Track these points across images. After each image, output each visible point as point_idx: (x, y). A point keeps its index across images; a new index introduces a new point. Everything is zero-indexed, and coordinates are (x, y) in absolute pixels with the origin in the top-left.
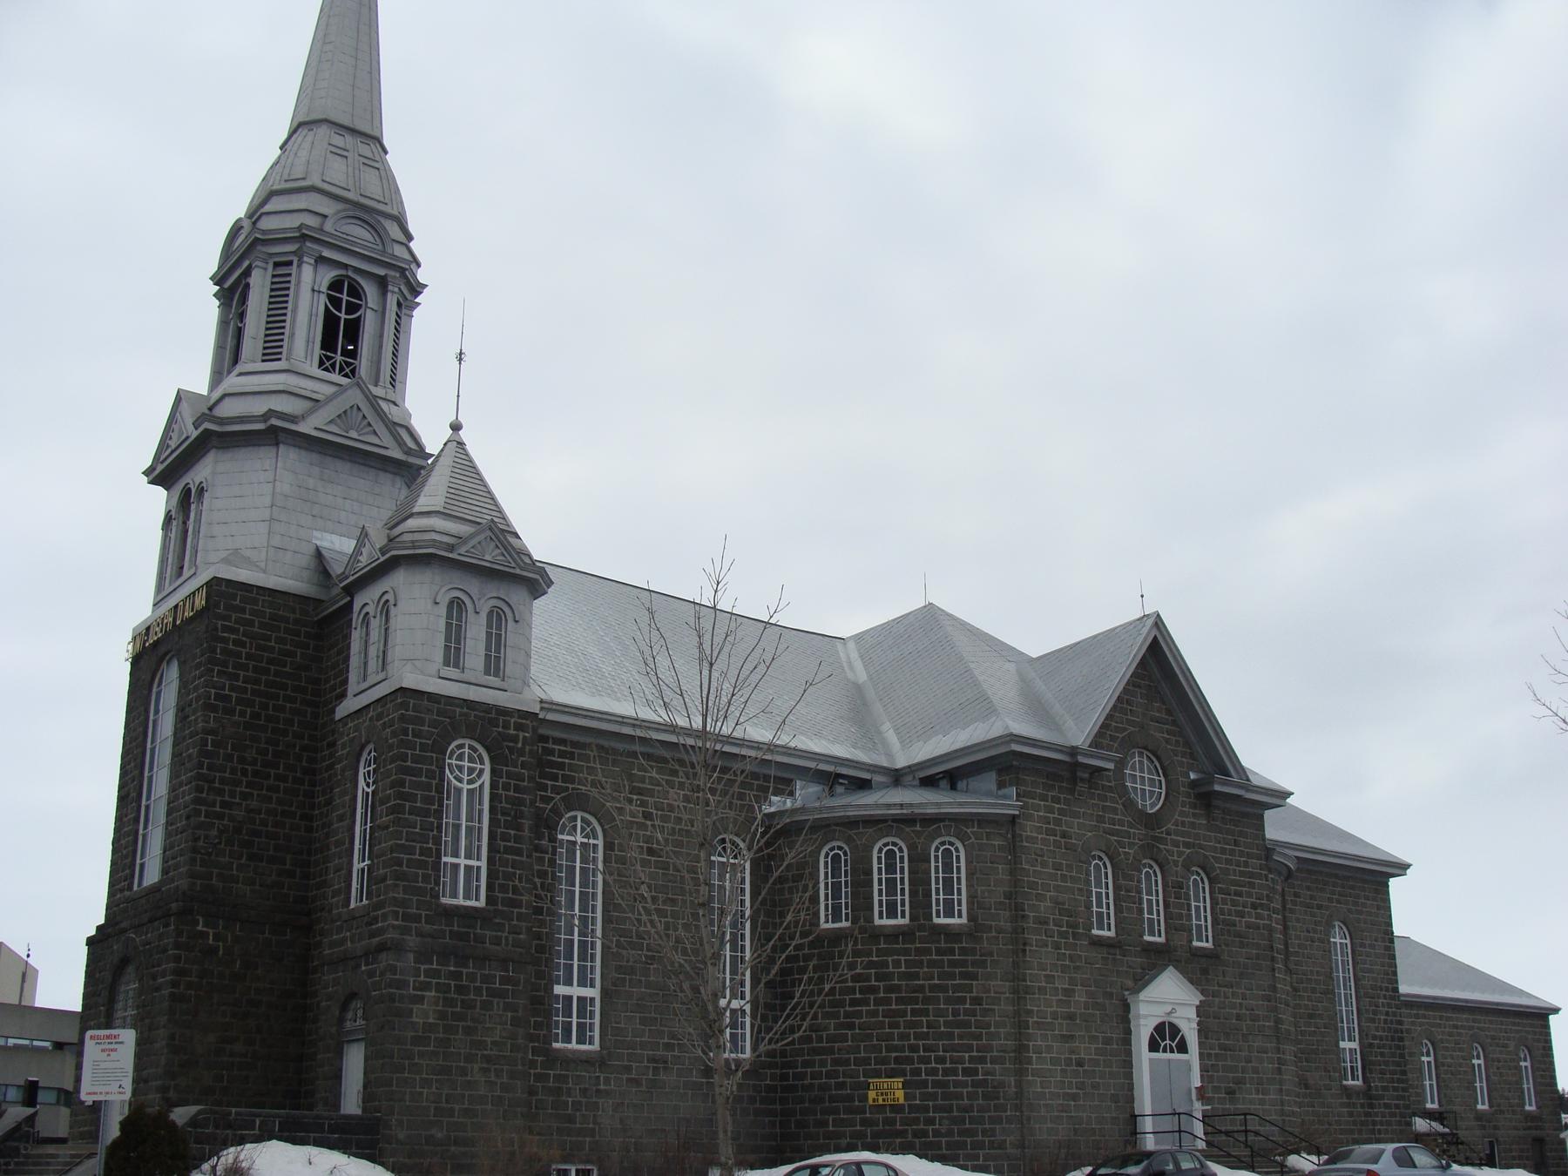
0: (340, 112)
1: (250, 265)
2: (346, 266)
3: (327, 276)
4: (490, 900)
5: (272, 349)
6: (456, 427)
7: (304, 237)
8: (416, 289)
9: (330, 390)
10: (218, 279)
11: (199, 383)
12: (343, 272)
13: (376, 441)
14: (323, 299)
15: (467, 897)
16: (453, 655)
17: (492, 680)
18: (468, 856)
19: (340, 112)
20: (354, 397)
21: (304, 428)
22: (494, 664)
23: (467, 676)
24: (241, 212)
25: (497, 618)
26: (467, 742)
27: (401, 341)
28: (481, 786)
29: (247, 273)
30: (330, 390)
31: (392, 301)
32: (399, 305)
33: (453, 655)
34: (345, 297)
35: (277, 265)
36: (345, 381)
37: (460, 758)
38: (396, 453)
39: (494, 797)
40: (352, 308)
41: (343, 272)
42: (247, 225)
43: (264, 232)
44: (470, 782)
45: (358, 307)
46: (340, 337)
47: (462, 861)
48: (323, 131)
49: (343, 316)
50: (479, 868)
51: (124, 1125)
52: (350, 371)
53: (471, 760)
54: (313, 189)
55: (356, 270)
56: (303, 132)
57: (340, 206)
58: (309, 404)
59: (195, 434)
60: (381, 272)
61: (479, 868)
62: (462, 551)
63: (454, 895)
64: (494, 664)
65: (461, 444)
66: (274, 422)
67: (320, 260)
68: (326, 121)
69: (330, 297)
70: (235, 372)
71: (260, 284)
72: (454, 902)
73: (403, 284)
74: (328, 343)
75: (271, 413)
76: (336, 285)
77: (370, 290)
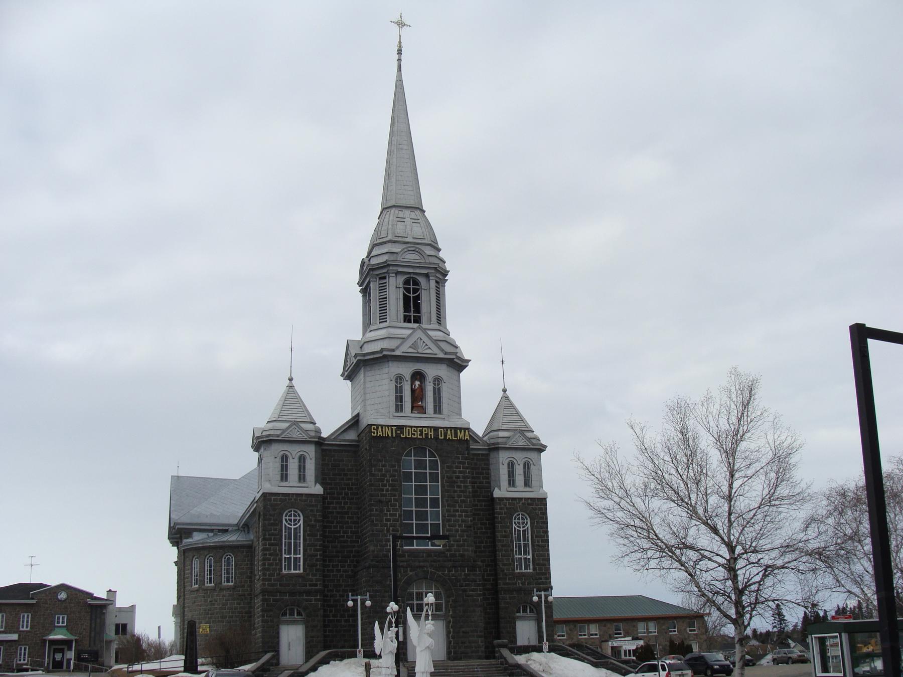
0: (402, 199)
1: (372, 275)
2: (410, 273)
3: (401, 279)
4: (534, 569)
5: (383, 319)
6: (291, 380)
8: (445, 273)
9: (409, 332)
10: (360, 284)
11: (358, 336)
14: (401, 291)
17: (528, 489)
19: (402, 199)
20: (419, 334)
21: (398, 353)
22: (527, 483)
24: (364, 255)
27: (441, 296)
29: (369, 283)
30: (409, 332)
31: (433, 284)
32: (437, 282)
34: (411, 287)
35: (380, 278)
36: (416, 325)
38: (441, 355)
40: (415, 291)
42: (366, 260)
46: (412, 309)
47: (523, 556)
48: (393, 210)
49: (412, 295)
51: (518, 666)
52: (417, 320)
53: (523, 519)
54: (390, 241)
55: (414, 273)
57: (405, 246)
60: (425, 271)
64: (527, 483)
65: (507, 397)
66: (385, 353)
67: (398, 273)
68: (394, 206)
69: (405, 288)
71: (374, 286)
73: (439, 274)
74: (407, 308)
75: (382, 350)
76: (407, 282)
77: (422, 281)
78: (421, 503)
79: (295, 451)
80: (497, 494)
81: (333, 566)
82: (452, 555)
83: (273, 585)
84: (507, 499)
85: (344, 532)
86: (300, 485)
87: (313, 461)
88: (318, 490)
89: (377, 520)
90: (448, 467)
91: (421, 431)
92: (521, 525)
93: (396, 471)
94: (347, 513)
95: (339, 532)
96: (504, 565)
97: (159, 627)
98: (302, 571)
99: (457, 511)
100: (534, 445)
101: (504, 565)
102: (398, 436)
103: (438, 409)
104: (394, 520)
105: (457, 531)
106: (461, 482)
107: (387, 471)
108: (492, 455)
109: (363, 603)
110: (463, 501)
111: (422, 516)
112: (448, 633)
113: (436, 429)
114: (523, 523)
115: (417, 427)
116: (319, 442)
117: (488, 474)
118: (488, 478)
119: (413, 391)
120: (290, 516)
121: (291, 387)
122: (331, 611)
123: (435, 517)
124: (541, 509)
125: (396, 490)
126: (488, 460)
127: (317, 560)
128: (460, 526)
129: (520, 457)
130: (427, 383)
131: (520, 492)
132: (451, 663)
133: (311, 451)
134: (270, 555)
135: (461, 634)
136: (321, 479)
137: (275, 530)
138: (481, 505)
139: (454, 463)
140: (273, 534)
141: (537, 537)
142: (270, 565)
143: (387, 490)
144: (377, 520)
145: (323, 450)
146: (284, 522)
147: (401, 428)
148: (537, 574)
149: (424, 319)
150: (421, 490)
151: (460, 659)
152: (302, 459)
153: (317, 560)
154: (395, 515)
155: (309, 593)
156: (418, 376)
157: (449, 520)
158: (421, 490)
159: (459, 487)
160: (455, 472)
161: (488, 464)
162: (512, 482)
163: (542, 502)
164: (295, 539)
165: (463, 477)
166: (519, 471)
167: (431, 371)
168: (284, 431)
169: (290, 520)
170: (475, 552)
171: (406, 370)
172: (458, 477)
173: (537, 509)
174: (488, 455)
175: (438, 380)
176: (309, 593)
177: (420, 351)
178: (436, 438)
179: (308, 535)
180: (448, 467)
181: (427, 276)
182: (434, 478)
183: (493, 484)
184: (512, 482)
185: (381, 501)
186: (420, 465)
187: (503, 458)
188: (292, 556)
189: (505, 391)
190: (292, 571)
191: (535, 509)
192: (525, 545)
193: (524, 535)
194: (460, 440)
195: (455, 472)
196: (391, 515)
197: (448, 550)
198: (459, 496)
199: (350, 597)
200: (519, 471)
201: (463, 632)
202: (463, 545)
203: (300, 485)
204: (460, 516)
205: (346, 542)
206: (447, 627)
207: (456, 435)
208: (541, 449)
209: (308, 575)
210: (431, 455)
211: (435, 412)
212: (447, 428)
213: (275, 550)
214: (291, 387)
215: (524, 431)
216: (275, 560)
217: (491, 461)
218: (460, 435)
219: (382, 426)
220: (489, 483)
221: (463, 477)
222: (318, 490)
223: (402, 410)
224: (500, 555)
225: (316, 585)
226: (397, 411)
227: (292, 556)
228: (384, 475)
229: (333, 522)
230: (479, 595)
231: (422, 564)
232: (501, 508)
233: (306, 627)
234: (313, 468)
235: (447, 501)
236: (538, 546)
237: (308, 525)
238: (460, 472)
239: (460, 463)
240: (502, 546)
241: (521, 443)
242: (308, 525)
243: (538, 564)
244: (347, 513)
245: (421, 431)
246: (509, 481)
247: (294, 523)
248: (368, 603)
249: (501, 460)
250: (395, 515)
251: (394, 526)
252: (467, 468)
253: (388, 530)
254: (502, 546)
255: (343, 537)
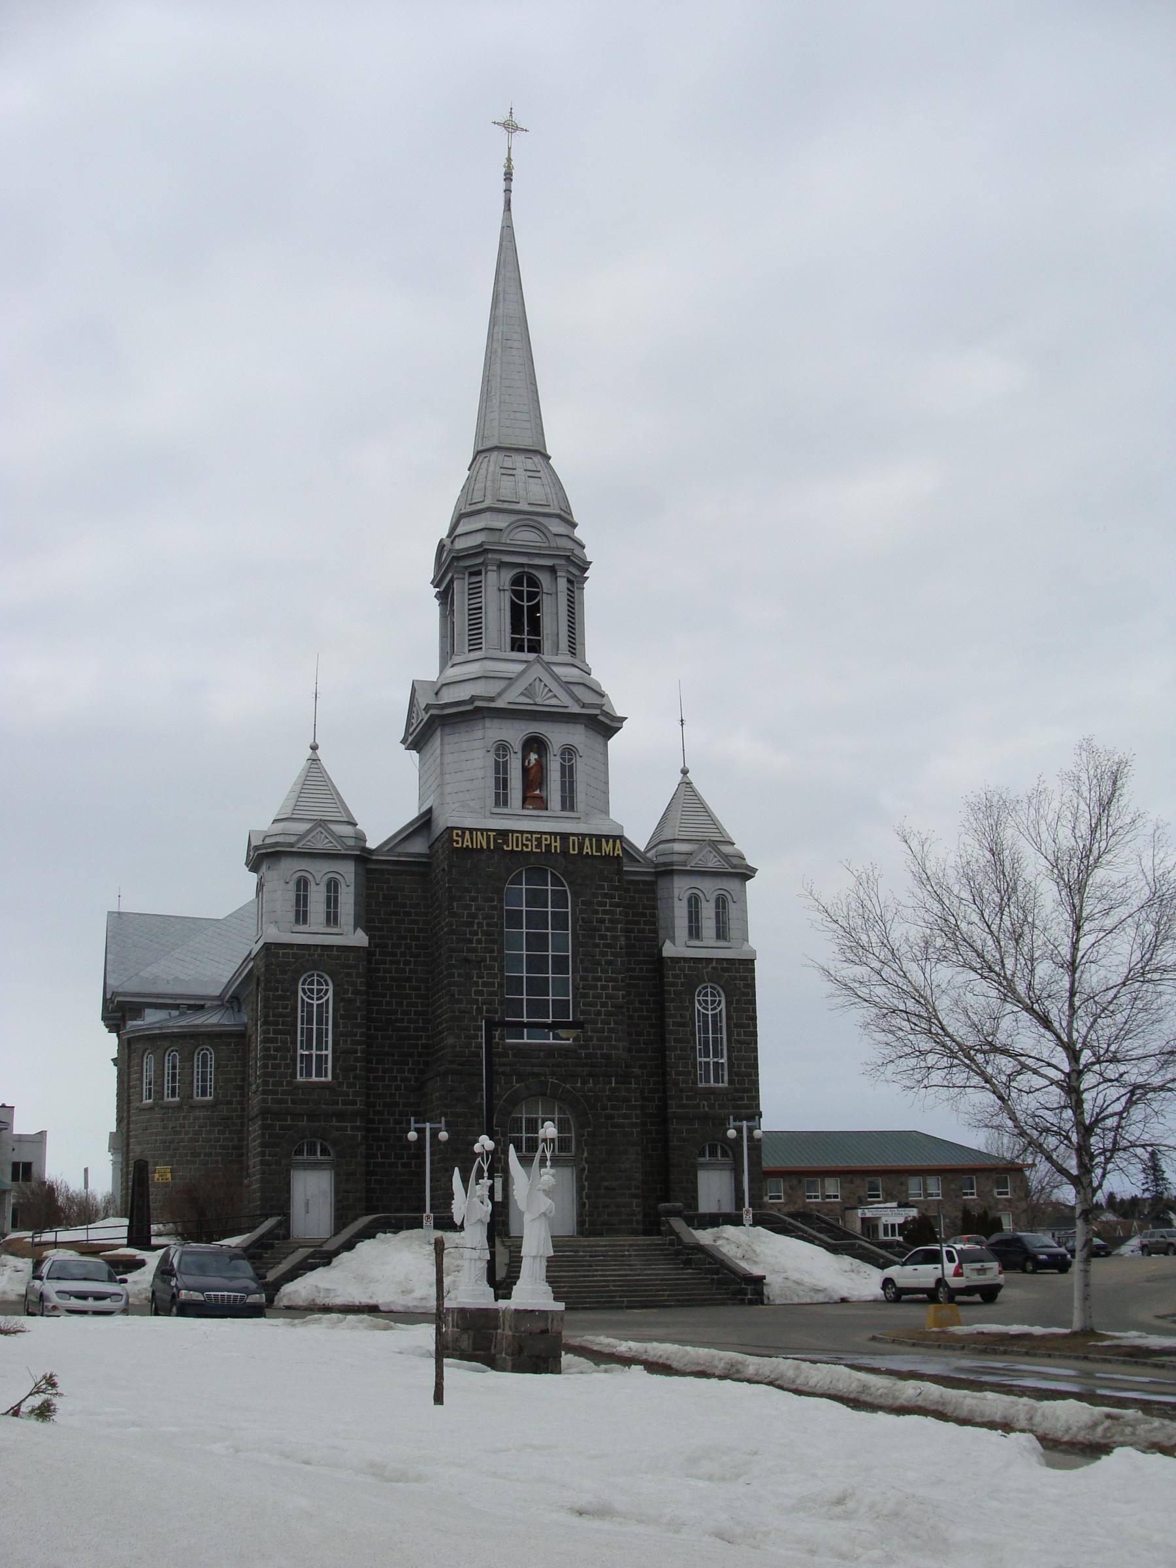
0: (510, 437)
2: (522, 565)
3: (507, 575)
4: (731, 1081)
5: (475, 643)
7: (486, 551)
8: (584, 566)
9: (520, 667)
12: (518, 570)
13: (559, 703)
14: (508, 594)
15: (318, 1075)
16: (301, 916)
18: (708, 1063)
19: (510, 437)
20: (538, 671)
21: (500, 704)
22: (722, 933)
23: (314, 929)
25: (721, 903)
26: (709, 985)
28: (327, 1001)
30: (520, 667)
31: (562, 584)
32: (570, 581)
33: (301, 916)
34: (525, 589)
37: (706, 995)
38: (576, 709)
39: (729, 1018)
40: (532, 596)
41: (518, 570)
42: (447, 542)
43: (459, 551)
44: (318, 999)
45: (537, 594)
46: (526, 628)
48: (494, 455)
49: (525, 604)
50: (326, 1056)
53: (713, 995)
56: (480, 458)
58: (507, 682)
59: (426, 717)
60: (549, 562)
61: (326, 1056)
62: (300, 845)
63: (309, 1074)
64: (722, 933)
67: (501, 565)
68: (496, 448)
69: (514, 591)
70: (450, 664)
72: (708, 1085)
73: (575, 567)
74: (516, 627)
75: (473, 699)
76: (517, 581)
77: (544, 578)
78: (537, 964)
79: (319, 871)
80: (669, 950)
81: (384, 1071)
82: (588, 1056)
83: (280, 1102)
84: (685, 960)
85: (405, 1013)
86: (329, 930)
87: (352, 889)
88: (360, 939)
89: (460, 993)
90: (583, 903)
91: (539, 840)
92: (709, 1005)
93: (494, 908)
94: (409, 980)
95: (395, 1012)
96: (678, 1074)
97: (438, 1398)
98: (726, 1085)
99: (600, 979)
100: (734, 867)
101: (678, 1074)
102: (498, 848)
103: (568, 802)
104: (491, 994)
105: (599, 1013)
106: (607, 929)
107: (478, 909)
108: (662, 883)
109: (434, 1134)
110: (609, 963)
111: (537, 987)
112: (580, 1189)
113: (564, 837)
114: (713, 1002)
115: (532, 833)
116: (363, 858)
117: (654, 915)
118: (654, 923)
119: (525, 770)
120: (312, 983)
121: (314, 761)
122: (379, 1148)
123: (561, 988)
124: (745, 979)
125: (494, 942)
126: (654, 892)
127: (357, 1060)
128: (604, 1005)
129: (709, 888)
130: (550, 757)
131: (708, 948)
132: (584, 1241)
133: (347, 872)
134: (276, 1049)
135: (602, 1191)
136: (365, 920)
137: (286, 1007)
138: (641, 969)
139: (595, 895)
140: (281, 1015)
141: (736, 1026)
142: (275, 1066)
143: (479, 942)
144: (460, 993)
145: (369, 871)
146: (300, 993)
147: (503, 834)
148: (737, 1090)
149: (547, 645)
150: (537, 942)
151: (601, 1234)
152: (333, 886)
153: (357, 1060)
154: (493, 984)
155: (340, 1116)
156: (535, 744)
157: (585, 996)
158: (537, 942)
159: (603, 937)
160: (597, 912)
161: (655, 899)
162: (695, 931)
163: (747, 965)
164: (320, 1022)
165: (611, 921)
166: (708, 911)
167: (557, 736)
168: (302, 837)
169: (311, 991)
170: (630, 1050)
171: (515, 734)
172: (602, 921)
173: (737, 979)
174: (654, 883)
175: (569, 752)
176: (340, 1116)
177: (539, 701)
178: (565, 852)
179: (342, 1017)
180: (583, 903)
181: (552, 570)
182: (560, 921)
183: (661, 933)
184: (695, 931)
185: (467, 960)
186: (536, 898)
187: (681, 888)
188: (314, 1052)
189: (685, 772)
190: (314, 1079)
191: (735, 978)
192: (715, 1040)
193: (715, 1023)
194: (607, 856)
195: (597, 912)
196: (485, 984)
197: (581, 1047)
198: (604, 954)
199: (413, 1125)
200: (708, 911)
201: (607, 1188)
202: (609, 1039)
203: (329, 930)
204: (604, 988)
205: (407, 1029)
206: (579, 1179)
207: (599, 849)
208: (746, 874)
209: (340, 1085)
210: (556, 881)
211: (563, 808)
212: (584, 836)
213: (284, 1042)
214: (314, 761)
215: (718, 842)
216: (284, 1058)
217: (660, 894)
218: (607, 848)
219: (471, 830)
220: (656, 932)
221: (611, 921)
222: (360, 939)
223: (505, 804)
224: (672, 1057)
225: (354, 1103)
226: (497, 804)
227: (314, 1052)
228: (474, 916)
229: (384, 996)
230: (634, 1125)
231: (536, 1069)
232: (674, 976)
233: (337, 1175)
234: (352, 901)
235: (582, 962)
236: (739, 1042)
237: (343, 1000)
238: (605, 912)
239: (605, 895)
240: (676, 1041)
241: (713, 863)
242: (343, 1000)
243: (737, 1074)
244: (409, 980)
245: (539, 840)
246: (690, 928)
247: (318, 995)
248: (443, 1135)
249: (676, 892)
250: (493, 984)
251: (491, 1003)
252: (618, 905)
253: (479, 1010)
254: (676, 1041)
255: (402, 1021)
